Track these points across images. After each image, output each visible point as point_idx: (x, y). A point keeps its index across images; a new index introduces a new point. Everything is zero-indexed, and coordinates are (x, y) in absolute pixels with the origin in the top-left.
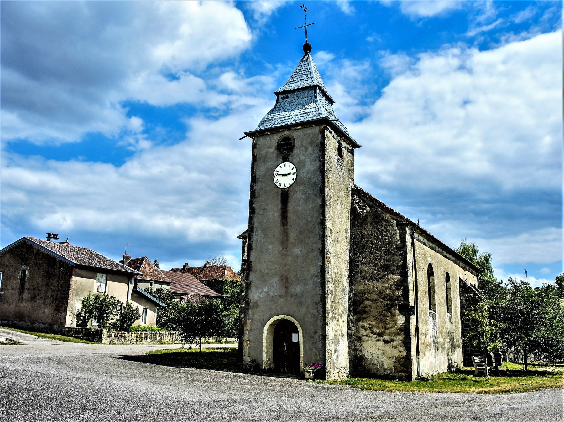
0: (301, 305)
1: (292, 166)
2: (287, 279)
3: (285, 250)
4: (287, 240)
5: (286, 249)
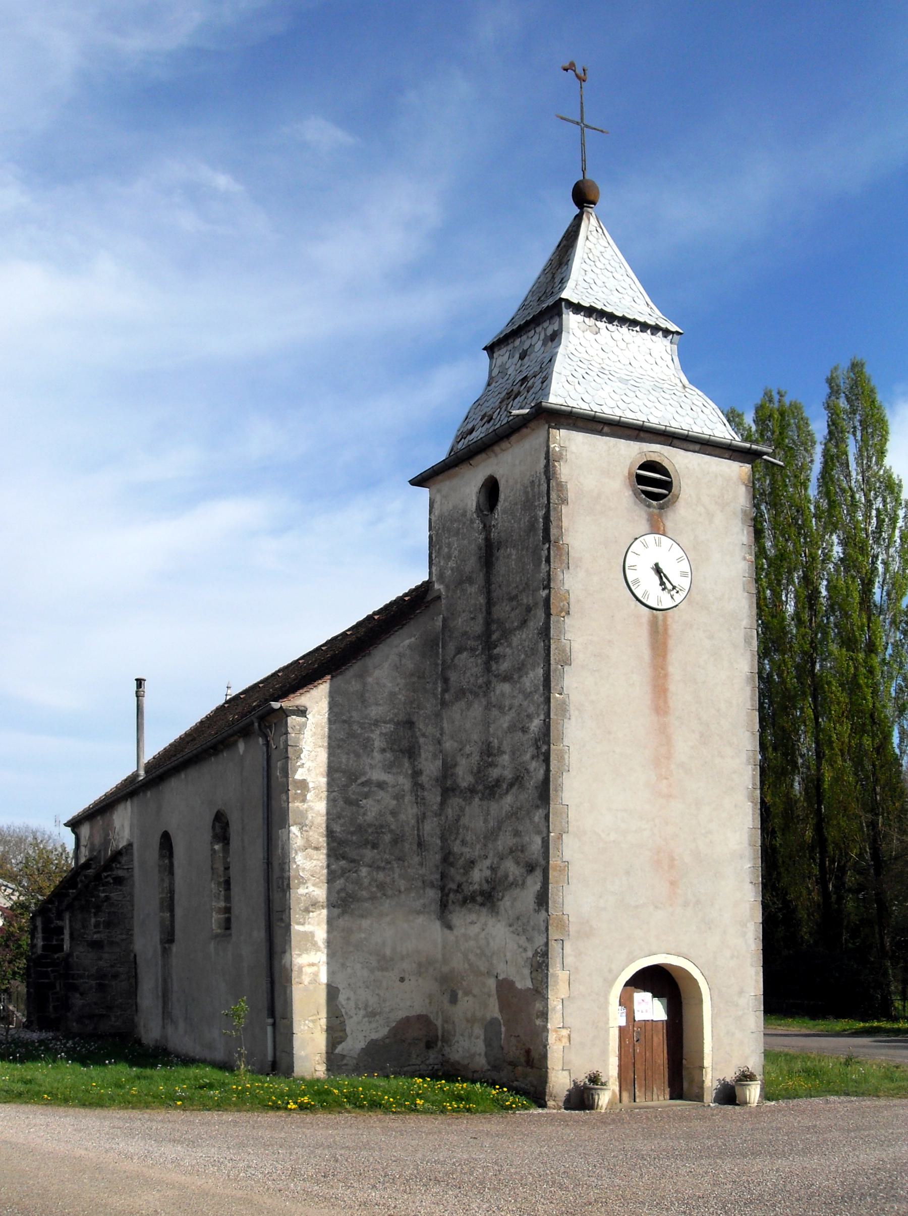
0: (710, 928)
1: (677, 552)
2: (672, 859)
3: (665, 781)
4: (669, 757)
5: (667, 779)
